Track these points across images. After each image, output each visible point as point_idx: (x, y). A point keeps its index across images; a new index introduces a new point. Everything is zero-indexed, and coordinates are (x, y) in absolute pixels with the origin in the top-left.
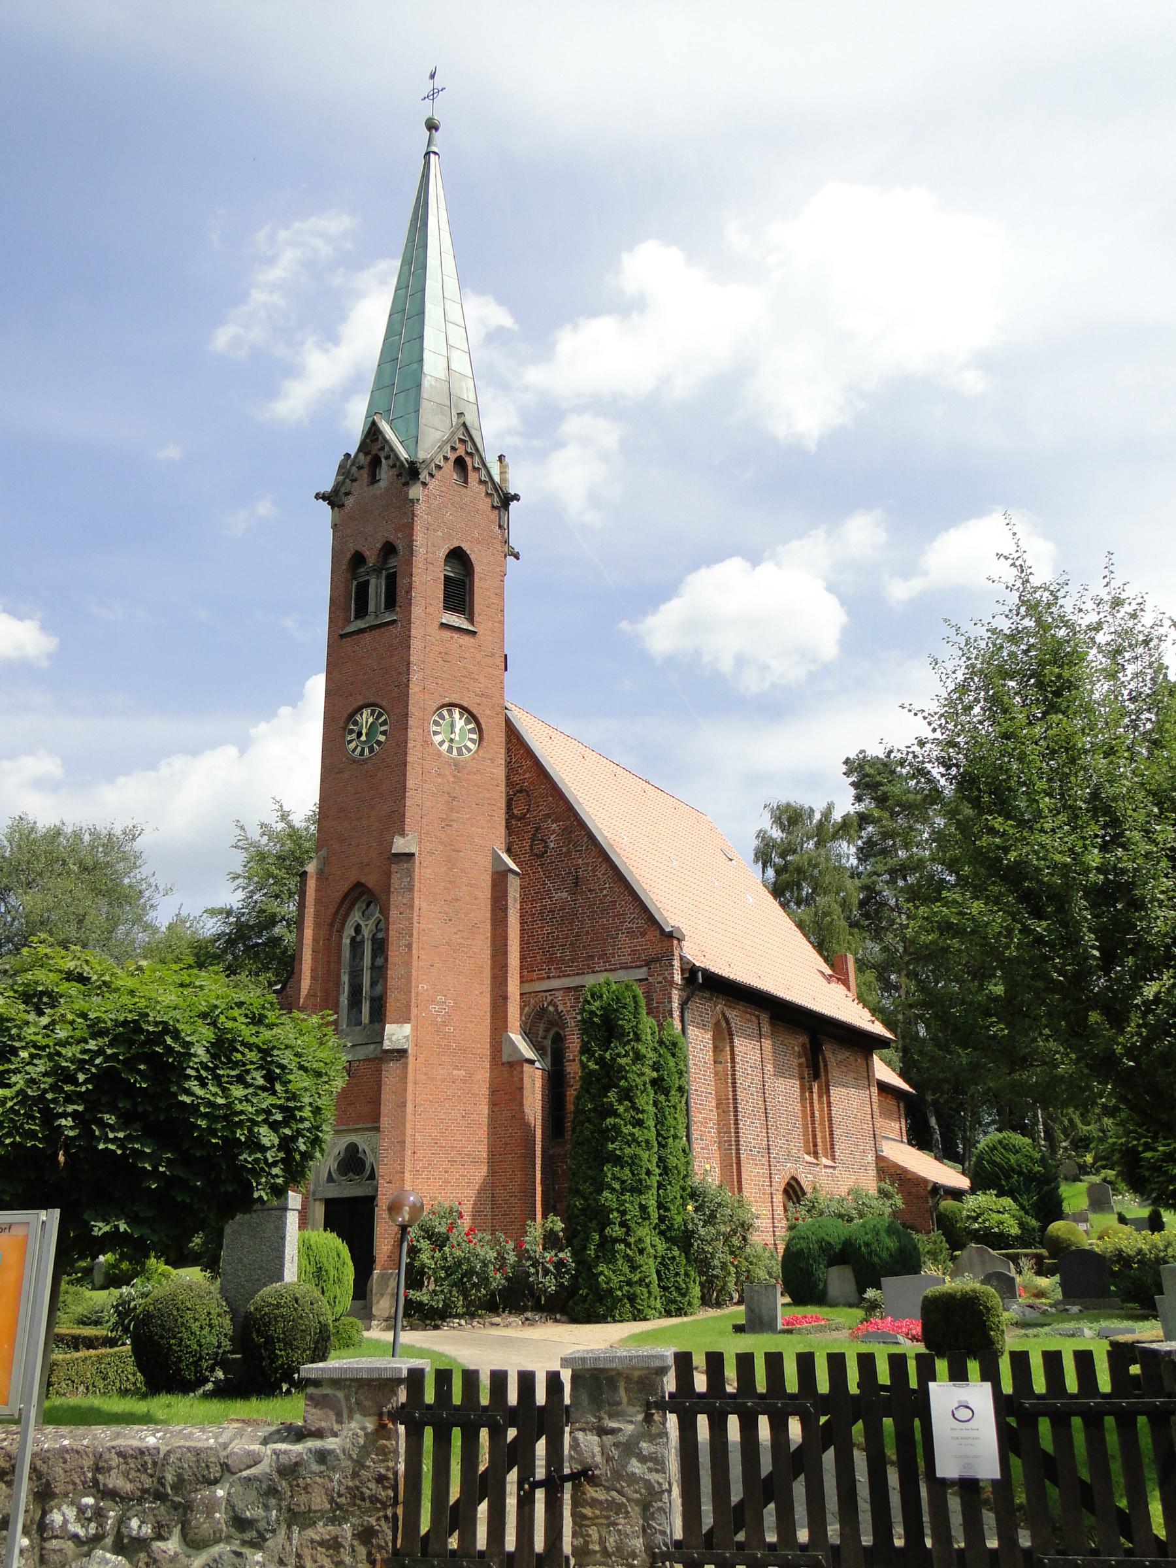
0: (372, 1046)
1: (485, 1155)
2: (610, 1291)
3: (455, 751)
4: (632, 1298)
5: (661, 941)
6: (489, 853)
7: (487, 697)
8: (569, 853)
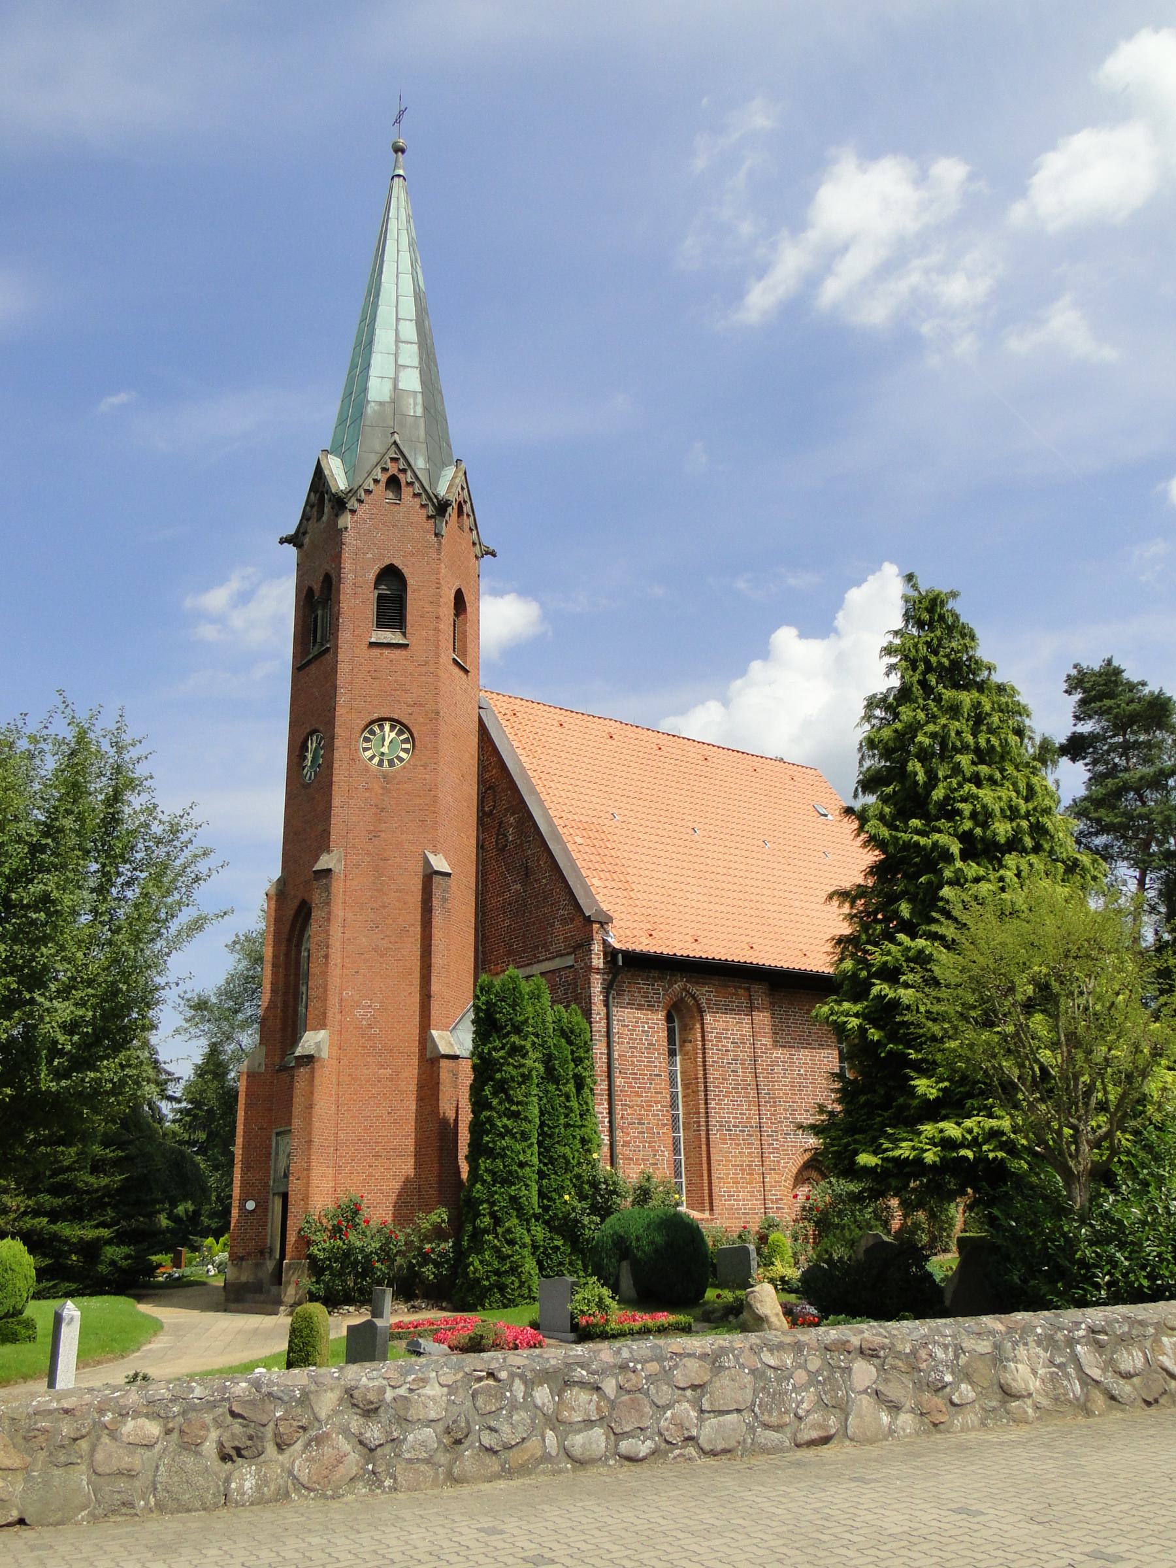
1: (412, 1149)
2: (478, 1281)
3: (386, 763)
4: (502, 1288)
6: (420, 858)
7: (421, 705)
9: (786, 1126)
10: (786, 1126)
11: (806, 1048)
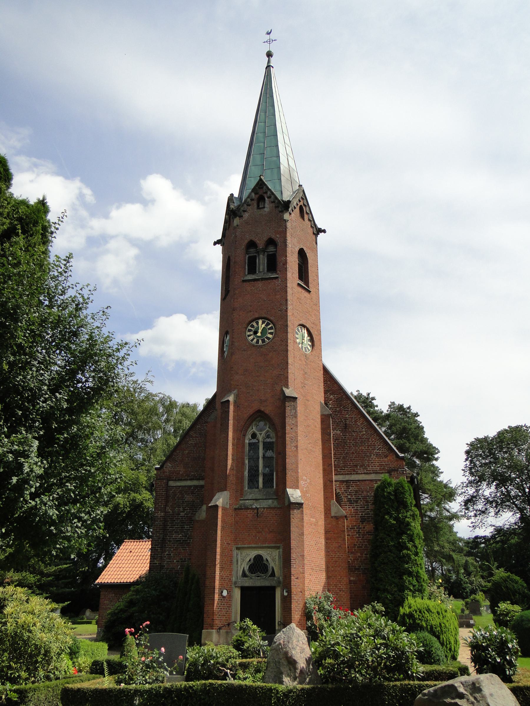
0: (270, 501)
5: (397, 461)
8: (340, 411)
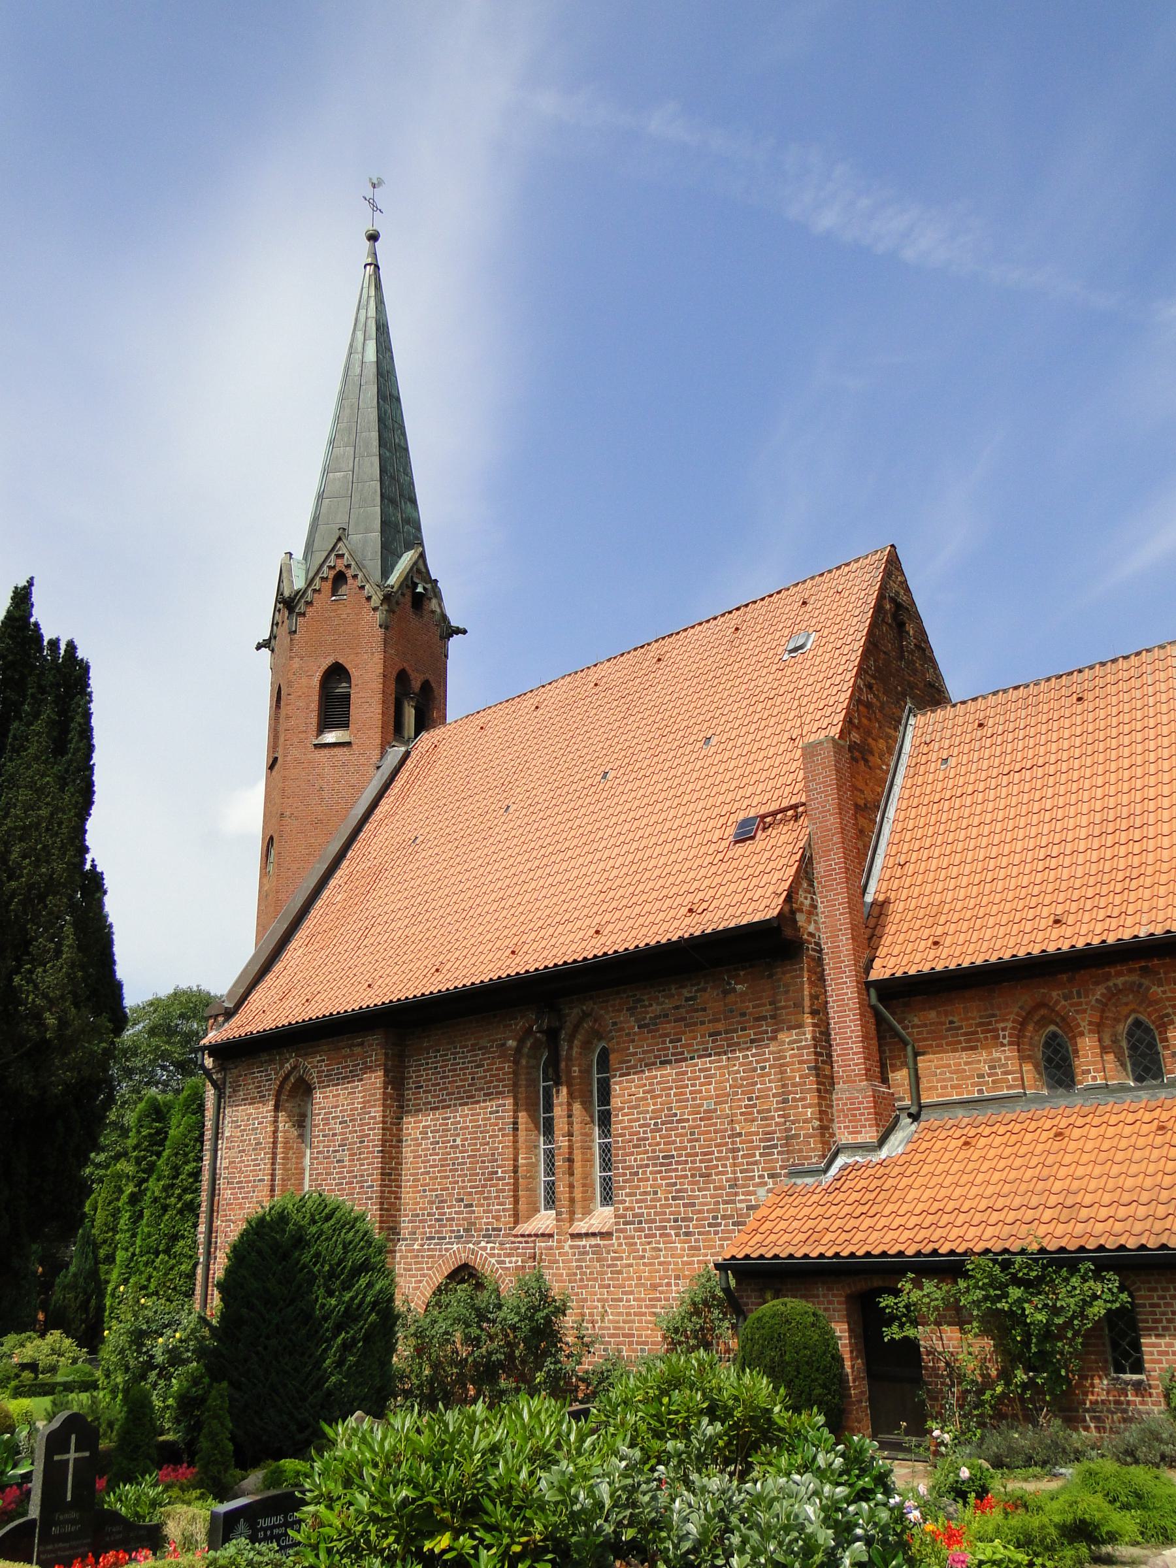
9: (429, 1227)
10: (429, 1227)
11: (466, 1104)
